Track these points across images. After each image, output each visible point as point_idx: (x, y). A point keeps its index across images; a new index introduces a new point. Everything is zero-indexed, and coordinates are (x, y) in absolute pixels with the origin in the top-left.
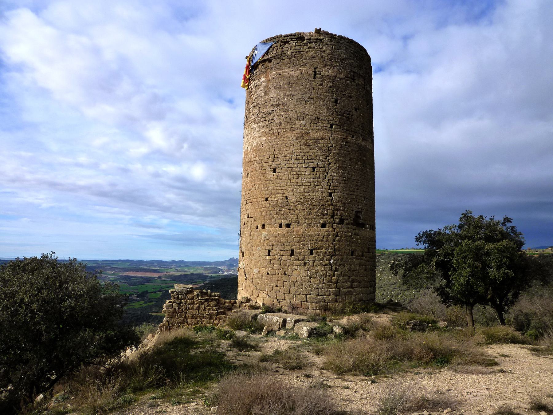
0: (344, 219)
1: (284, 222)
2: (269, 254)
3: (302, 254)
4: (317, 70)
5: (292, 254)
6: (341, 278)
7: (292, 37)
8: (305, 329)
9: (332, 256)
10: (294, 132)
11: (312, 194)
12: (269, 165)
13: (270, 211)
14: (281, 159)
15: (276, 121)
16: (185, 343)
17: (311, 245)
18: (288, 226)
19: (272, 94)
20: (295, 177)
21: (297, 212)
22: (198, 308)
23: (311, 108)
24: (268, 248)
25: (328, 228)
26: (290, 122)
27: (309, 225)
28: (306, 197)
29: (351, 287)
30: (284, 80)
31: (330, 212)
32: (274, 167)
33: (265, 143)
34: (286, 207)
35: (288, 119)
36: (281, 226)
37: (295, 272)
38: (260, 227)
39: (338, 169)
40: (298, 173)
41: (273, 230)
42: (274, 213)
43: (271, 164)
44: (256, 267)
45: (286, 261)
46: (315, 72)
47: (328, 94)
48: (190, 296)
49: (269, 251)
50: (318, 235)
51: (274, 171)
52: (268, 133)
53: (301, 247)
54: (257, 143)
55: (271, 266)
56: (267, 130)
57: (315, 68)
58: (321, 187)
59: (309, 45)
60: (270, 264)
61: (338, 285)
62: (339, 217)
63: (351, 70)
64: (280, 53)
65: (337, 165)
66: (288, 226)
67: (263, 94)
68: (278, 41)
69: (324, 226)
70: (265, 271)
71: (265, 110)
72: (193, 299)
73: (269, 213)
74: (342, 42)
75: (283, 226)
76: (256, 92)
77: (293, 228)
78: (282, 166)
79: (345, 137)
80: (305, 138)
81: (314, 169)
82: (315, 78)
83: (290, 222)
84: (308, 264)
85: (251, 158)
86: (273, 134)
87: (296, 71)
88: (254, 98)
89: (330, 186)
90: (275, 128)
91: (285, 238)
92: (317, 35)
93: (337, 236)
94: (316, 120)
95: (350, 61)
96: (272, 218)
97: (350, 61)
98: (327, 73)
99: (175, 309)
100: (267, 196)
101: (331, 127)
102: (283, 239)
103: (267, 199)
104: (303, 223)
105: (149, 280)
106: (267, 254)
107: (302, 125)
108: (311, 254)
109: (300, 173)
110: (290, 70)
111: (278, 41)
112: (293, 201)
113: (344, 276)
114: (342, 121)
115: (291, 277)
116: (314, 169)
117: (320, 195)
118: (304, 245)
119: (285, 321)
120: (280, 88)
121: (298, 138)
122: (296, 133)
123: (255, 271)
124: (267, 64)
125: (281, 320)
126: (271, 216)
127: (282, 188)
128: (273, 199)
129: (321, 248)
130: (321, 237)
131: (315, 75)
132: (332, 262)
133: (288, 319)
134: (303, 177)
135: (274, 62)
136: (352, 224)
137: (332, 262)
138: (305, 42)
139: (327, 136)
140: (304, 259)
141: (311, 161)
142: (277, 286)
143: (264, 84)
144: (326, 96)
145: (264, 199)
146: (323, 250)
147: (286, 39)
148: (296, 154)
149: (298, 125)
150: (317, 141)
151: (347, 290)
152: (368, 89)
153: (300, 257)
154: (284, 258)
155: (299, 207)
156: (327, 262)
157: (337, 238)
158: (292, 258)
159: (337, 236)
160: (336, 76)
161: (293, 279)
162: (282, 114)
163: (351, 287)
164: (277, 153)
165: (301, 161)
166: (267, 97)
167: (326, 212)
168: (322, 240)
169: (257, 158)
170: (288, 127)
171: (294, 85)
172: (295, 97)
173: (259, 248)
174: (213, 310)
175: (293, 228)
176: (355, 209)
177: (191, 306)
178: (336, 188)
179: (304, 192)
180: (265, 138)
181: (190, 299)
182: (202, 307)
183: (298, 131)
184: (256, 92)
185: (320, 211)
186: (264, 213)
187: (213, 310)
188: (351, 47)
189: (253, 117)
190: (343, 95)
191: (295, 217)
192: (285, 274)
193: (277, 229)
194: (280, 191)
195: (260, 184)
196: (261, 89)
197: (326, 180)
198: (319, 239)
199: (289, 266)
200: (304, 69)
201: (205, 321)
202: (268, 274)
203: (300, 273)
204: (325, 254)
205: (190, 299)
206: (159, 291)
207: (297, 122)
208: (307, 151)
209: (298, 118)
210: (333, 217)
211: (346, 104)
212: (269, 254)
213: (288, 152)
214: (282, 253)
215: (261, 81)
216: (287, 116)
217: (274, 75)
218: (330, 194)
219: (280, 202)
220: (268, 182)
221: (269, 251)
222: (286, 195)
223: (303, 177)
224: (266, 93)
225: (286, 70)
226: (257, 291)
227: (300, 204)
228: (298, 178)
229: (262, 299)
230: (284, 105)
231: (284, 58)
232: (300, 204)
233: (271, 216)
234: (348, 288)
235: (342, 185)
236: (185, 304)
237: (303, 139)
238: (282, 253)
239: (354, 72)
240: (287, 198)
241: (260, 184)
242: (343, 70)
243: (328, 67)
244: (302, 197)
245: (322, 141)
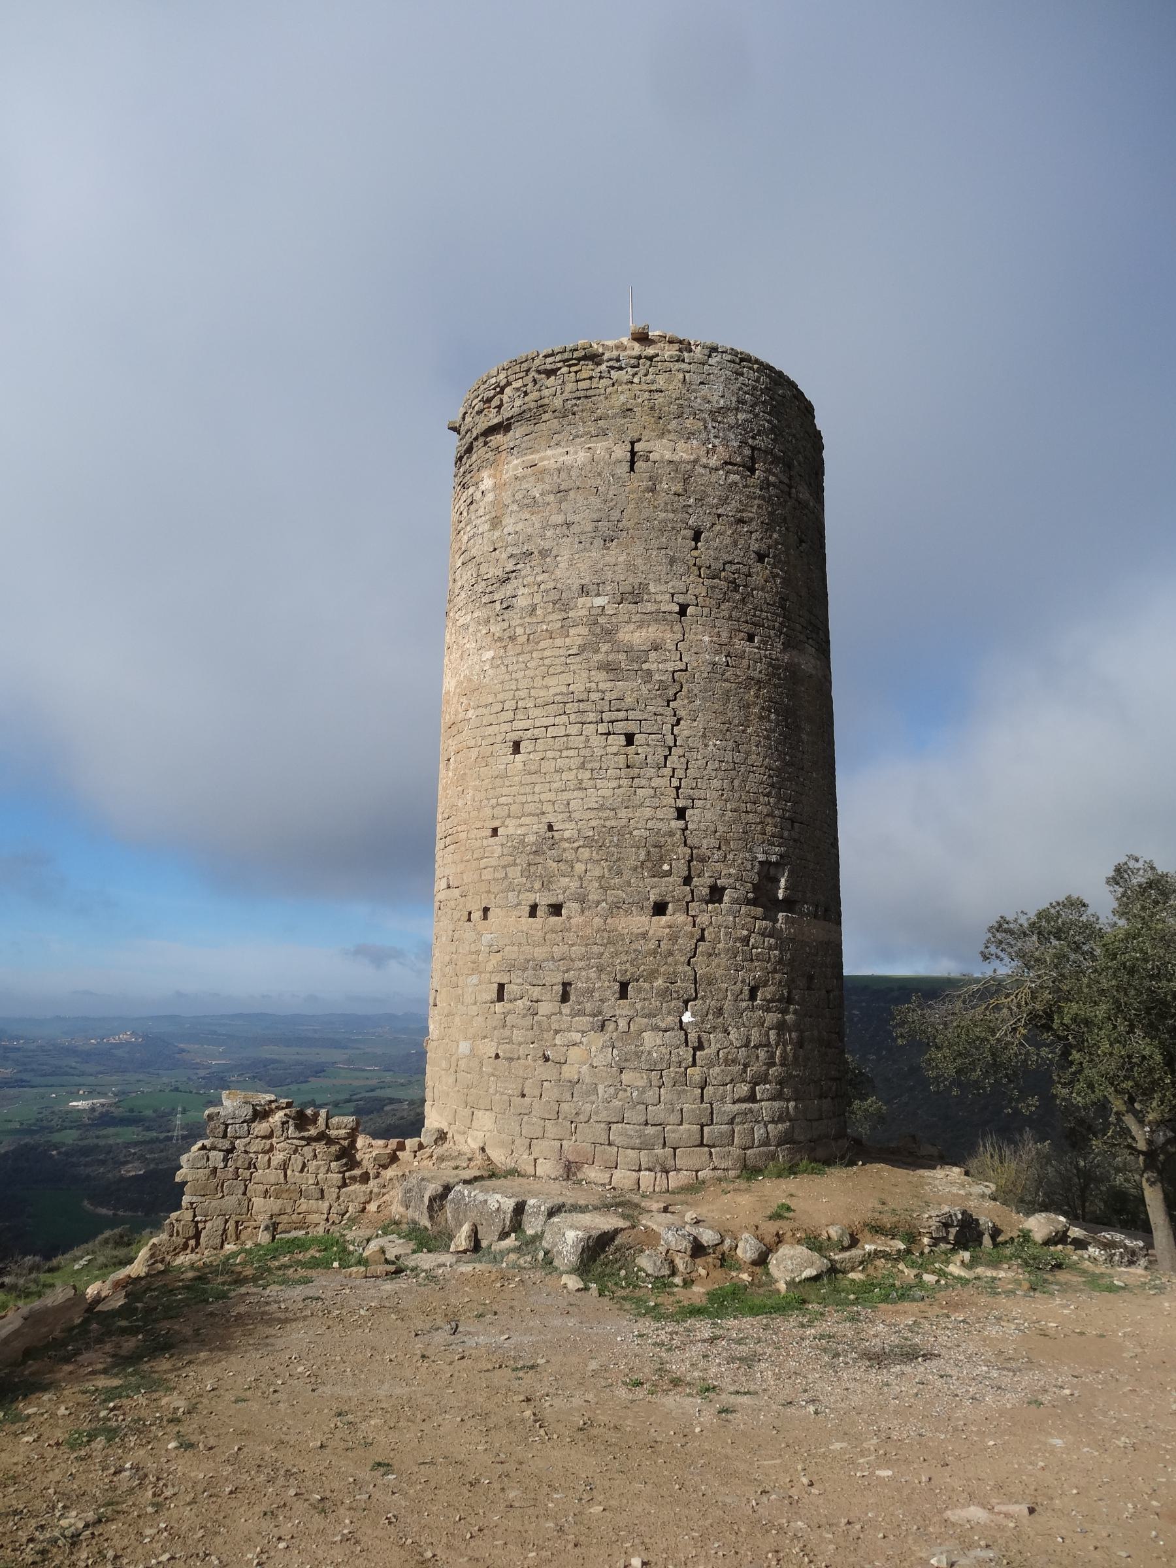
0: (724, 889)
1: (544, 900)
2: (500, 998)
3: (596, 995)
4: (638, 447)
5: (565, 998)
6: (717, 1069)
7: (566, 356)
8: (571, 1235)
9: (686, 1002)
10: (572, 631)
11: (623, 813)
12: (502, 732)
13: (504, 867)
14: (534, 713)
15: (522, 602)
16: (160, 1274)
17: (621, 966)
18: (556, 909)
19: (510, 524)
20: (577, 762)
21: (579, 867)
22: (284, 1167)
23: (621, 559)
24: (499, 979)
25: (675, 917)
26: (562, 604)
27: (616, 906)
28: (608, 824)
29: (752, 1098)
30: (542, 480)
31: (681, 868)
32: (514, 736)
33: (492, 667)
34: (549, 853)
35: (554, 595)
36: (533, 911)
37: (574, 1054)
38: (477, 915)
39: (704, 736)
40: (583, 752)
41: (509, 922)
42: (515, 873)
43: (506, 727)
44: (466, 1038)
45: (549, 1017)
46: (633, 453)
47: (671, 515)
48: (261, 1127)
49: (501, 987)
50: (644, 936)
51: (516, 747)
52: (500, 639)
53: (593, 974)
54: (471, 668)
55: (507, 1032)
56: (496, 629)
57: (633, 444)
58: (651, 792)
59: (615, 374)
60: (504, 1026)
61: (709, 1090)
62: (709, 882)
63: (744, 442)
64: (533, 405)
65: (700, 723)
66: (556, 909)
67: (487, 527)
68: (528, 371)
69: (660, 909)
70: (489, 1048)
71: (493, 572)
72: (270, 1136)
73: (500, 874)
74: (712, 361)
75: (540, 912)
76: (469, 522)
77: (569, 918)
78: (536, 731)
79: (724, 640)
80: (605, 647)
81: (630, 739)
82: (632, 469)
83: (561, 897)
84: (610, 1027)
85: (456, 713)
86: (512, 638)
87: (576, 453)
88: (465, 538)
89: (678, 788)
90: (519, 622)
91: (546, 949)
92: (636, 345)
93: (702, 939)
94: (635, 596)
95: (741, 416)
96: (510, 888)
97: (741, 416)
98: (668, 456)
99: (215, 1168)
100: (496, 824)
101: (683, 611)
102: (540, 952)
103: (495, 832)
104: (598, 903)
105: (319, 1070)
106: (495, 996)
107: (594, 612)
108: (623, 994)
109: (587, 752)
110: (561, 450)
111: (528, 371)
112: (567, 834)
113: (727, 1062)
114: (718, 594)
115: (565, 1067)
116: (630, 739)
117: (650, 816)
118: (600, 969)
119: (519, 1209)
120: (531, 504)
121: (583, 649)
122: (578, 635)
123: (464, 1047)
124: (497, 439)
125: (509, 1204)
126: (506, 883)
127: (536, 798)
128: (511, 831)
129: (652, 975)
130: (652, 945)
131: (632, 463)
132: (687, 1018)
133: (532, 1202)
134: (597, 765)
135: (518, 431)
136: (749, 903)
137: (687, 1018)
138: (603, 367)
139: (669, 638)
140: (600, 1013)
141: (622, 715)
142: (523, 1096)
143: (490, 497)
144: (665, 521)
145: (489, 832)
146: (659, 983)
147: (549, 364)
148: (578, 696)
149: (584, 612)
150: (638, 655)
151: (737, 1106)
152: (804, 494)
153: (589, 1007)
154: (544, 1008)
155: (585, 853)
156: (670, 1020)
157: (702, 947)
158: (566, 1009)
159: (702, 939)
160: (696, 461)
161: (569, 1072)
162: (539, 579)
163: (752, 1098)
164: (522, 694)
165: (592, 717)
166: (497, 534)
167: (666, 867)
168: (654, 953)
169: (470, 713)
170: (556, 616)
171: (571, 493)
172: (575, 529)
173: (474, 979)
174: (328, 1170)
175: (569, 918)
176: (761, 857)
177: (262, 1159)
178: (696, 793)
179: (602, 807)
180: (489, 654)
181: (263, 1137)
182: (297, 1161)
183: (584, 630)
184: (469, 522)
185: (649, 864)
186: (487, 875)
187: (328, 1170)
188: (742, 374)
189: (463, 595)
190: (719, 516)
191: (574, 885)
192: (547, 1059)
193: (523, 920)
194: (531, 808)
195: (476, 789)
196: (481, 512)
197: (667, 771)
198: (645, 948)
199: (557, 1032)
200: (600, 447)
201: (304, 1205)
202: (497, 1056)
203: (585, 1053)
204: (664, 994)
205: (263, 1137)
206: (349, 1101)
207: (581, 600)
208: (609, 685)
209: (584, 591)
210: (687, 881)
211: (728, 541)
212: (500, 998)
213: (552, 691)
214: (536, 992)
215: (482, 487)
216: (552, 585)
217: (516, 468)
218: (681, 813)
219: (531, 839)
220: (499, 781)
221: (501, 987)
222: (550, 818)
223: (597, 765)
224: (496, 523)
225: (549, 452)
226: (468, 1111)
227: (589, 842)
228: (582, 766)
229: (481, 1134)
230: (544, 554)
231: (545, 417)
232: (589, 842)
233: (506, 883)
234: (740, 1100)
235: (716, 783)
236: (246, 1152)
237: (597, 651)
238: (536, 992)
239: (753, 448)
240: (550, 828)
241: (476, 789)
242: (716, 442)
243: (672, 436)
244: (594, 823)
245: (653, 655)
